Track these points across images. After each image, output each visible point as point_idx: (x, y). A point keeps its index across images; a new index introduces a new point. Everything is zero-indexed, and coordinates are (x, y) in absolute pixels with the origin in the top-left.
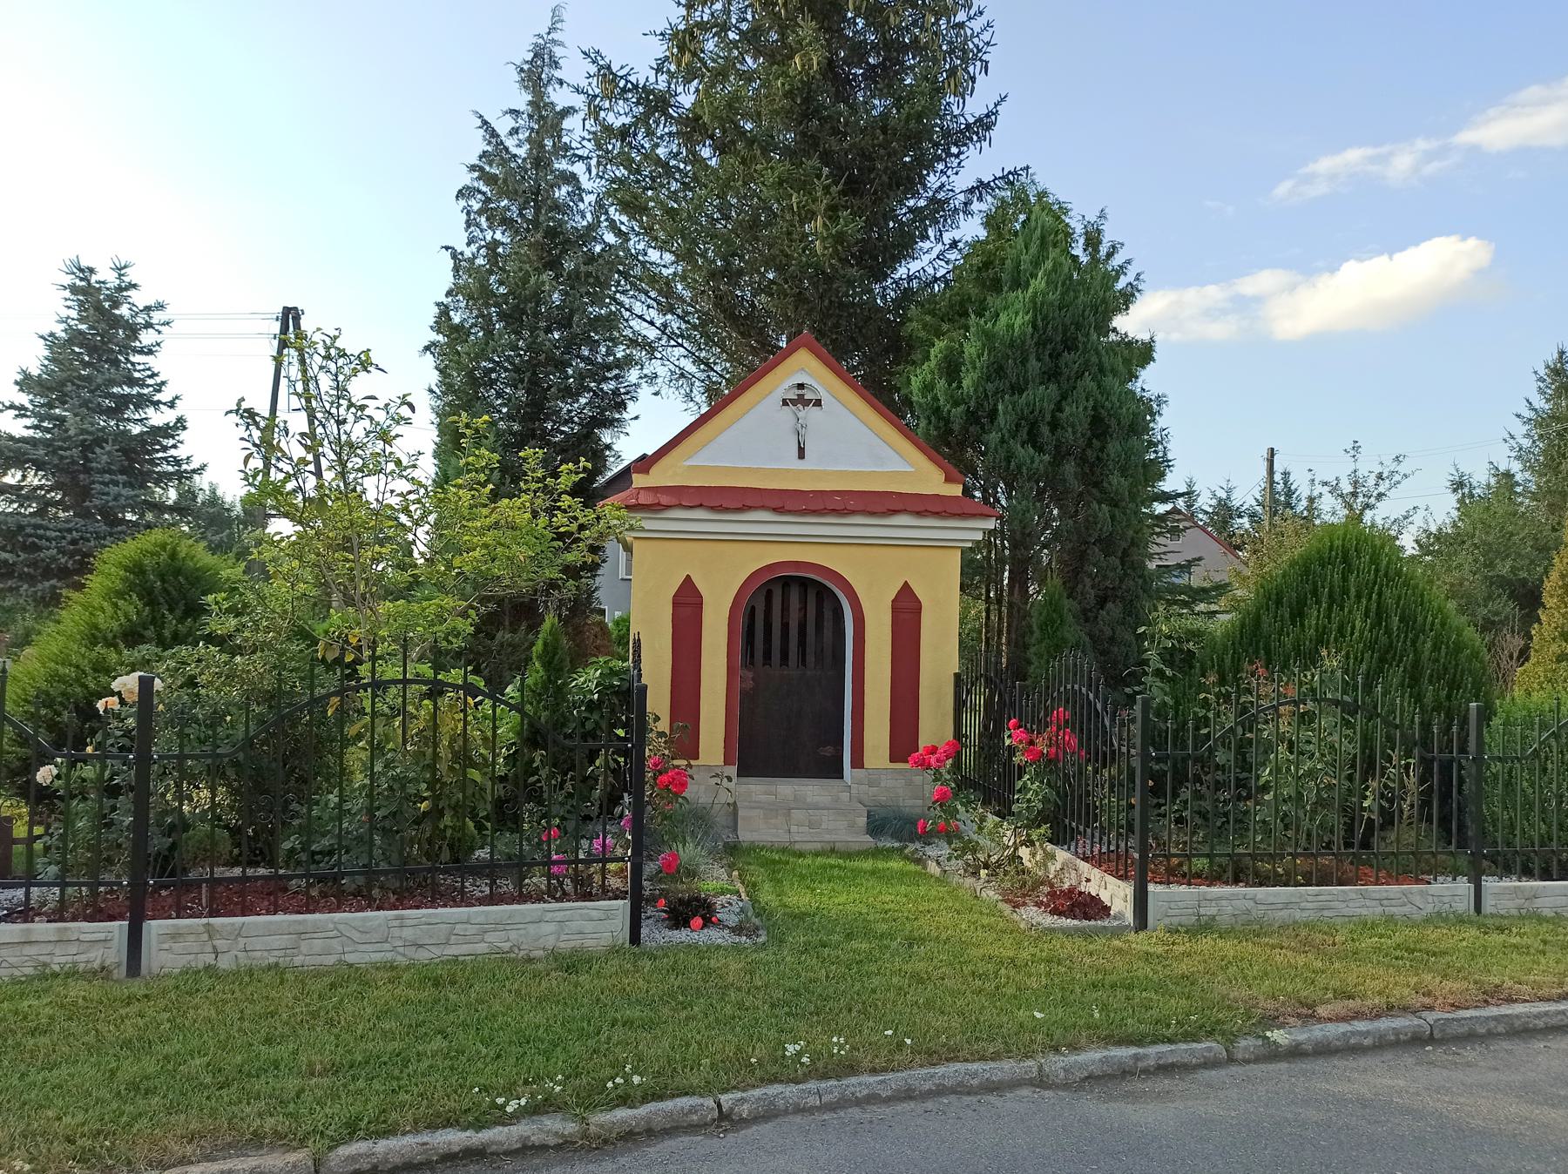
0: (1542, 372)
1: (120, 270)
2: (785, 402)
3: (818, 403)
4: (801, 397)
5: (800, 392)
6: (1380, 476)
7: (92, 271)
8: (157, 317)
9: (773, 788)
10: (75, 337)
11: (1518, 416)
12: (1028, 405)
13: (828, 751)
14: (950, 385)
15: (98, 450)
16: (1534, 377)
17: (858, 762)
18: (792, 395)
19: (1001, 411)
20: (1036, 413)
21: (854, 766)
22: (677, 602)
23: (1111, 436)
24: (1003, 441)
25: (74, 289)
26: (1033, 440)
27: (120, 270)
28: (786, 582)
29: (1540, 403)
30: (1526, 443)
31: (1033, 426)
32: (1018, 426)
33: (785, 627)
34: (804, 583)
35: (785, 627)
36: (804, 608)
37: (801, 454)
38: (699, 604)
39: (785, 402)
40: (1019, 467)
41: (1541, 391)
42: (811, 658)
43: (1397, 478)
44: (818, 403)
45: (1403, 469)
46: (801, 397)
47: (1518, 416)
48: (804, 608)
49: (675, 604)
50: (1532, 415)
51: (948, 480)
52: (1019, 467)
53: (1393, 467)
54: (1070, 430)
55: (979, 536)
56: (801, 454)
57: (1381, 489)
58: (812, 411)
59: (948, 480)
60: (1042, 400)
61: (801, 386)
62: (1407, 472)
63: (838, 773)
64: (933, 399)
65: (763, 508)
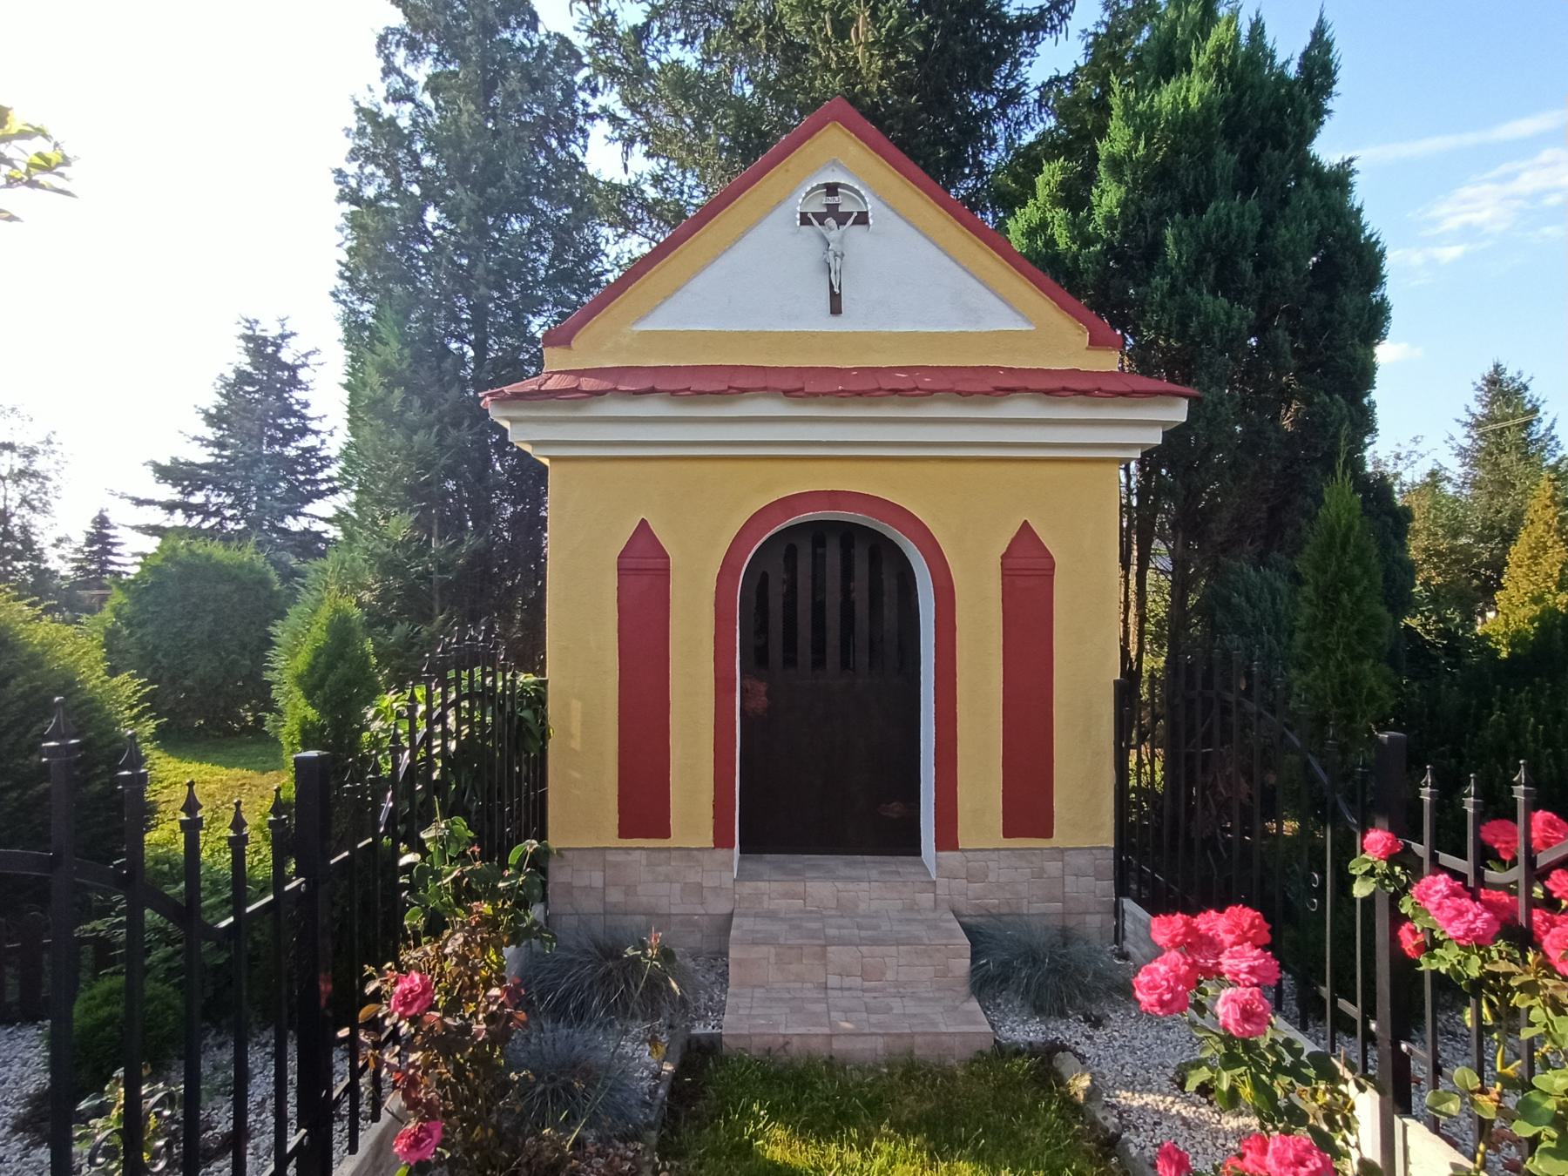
0: (1480, 383)
1: (282, 322)
2: (805, 220)
3: (862, 219)
4: (832, 210)
5: (831, 200)
6: (1398, 457)
7: (257, 322)
8: (312, 360)
9: (799, 887)
10: (243, 377)
11: (1458, 421)
12: (1218, 223)
13: (895, 809)
14: (1075, 215)
15: (256, 470)
16: (1473, 387)
17: (947, 839)
18: (818, 205)
19: (1170, 241)
20: (1232, 238)
21: (940, 846)
22: (625, 568)
23: (1345, 284)
24: (1173, 290)
25: (247, 338)
26: (1226, 284)
27: (282, 322)
28: (818, 532)
29: (1478, 409)
30: (1467, 443)
31: (1226, 263)
32: (1200, 262)
33: (819, 609)
34: (849, 534)
35: (819, 609)
36: (847, 573)
37: (836, 308)
38: (662, 572)
39: (805, 220)
40: (1205, 331)
41: (1480, 400)
42: (862, 658)
43: (1414, 457)
44: (862, 219)
45: (1421, 449)
46: (832, 210)
47: (1458, 421)
48: (847, 573)
49: (621, 570)
50: (1470, 419)
51: (1095, 343)
52: (1205, 331)
53: (1412, 447)
54: (1289, 265)
55: (1155, 438)
56: (836, 308)
57: (1399, 469)
58: (853, 232)
59: (1095, 343)
60: (1241, 216)
61: (832, 189)
62: (1424, 452)
63: (908, 844)
64: (1046, 244)
65: (766, 391)
